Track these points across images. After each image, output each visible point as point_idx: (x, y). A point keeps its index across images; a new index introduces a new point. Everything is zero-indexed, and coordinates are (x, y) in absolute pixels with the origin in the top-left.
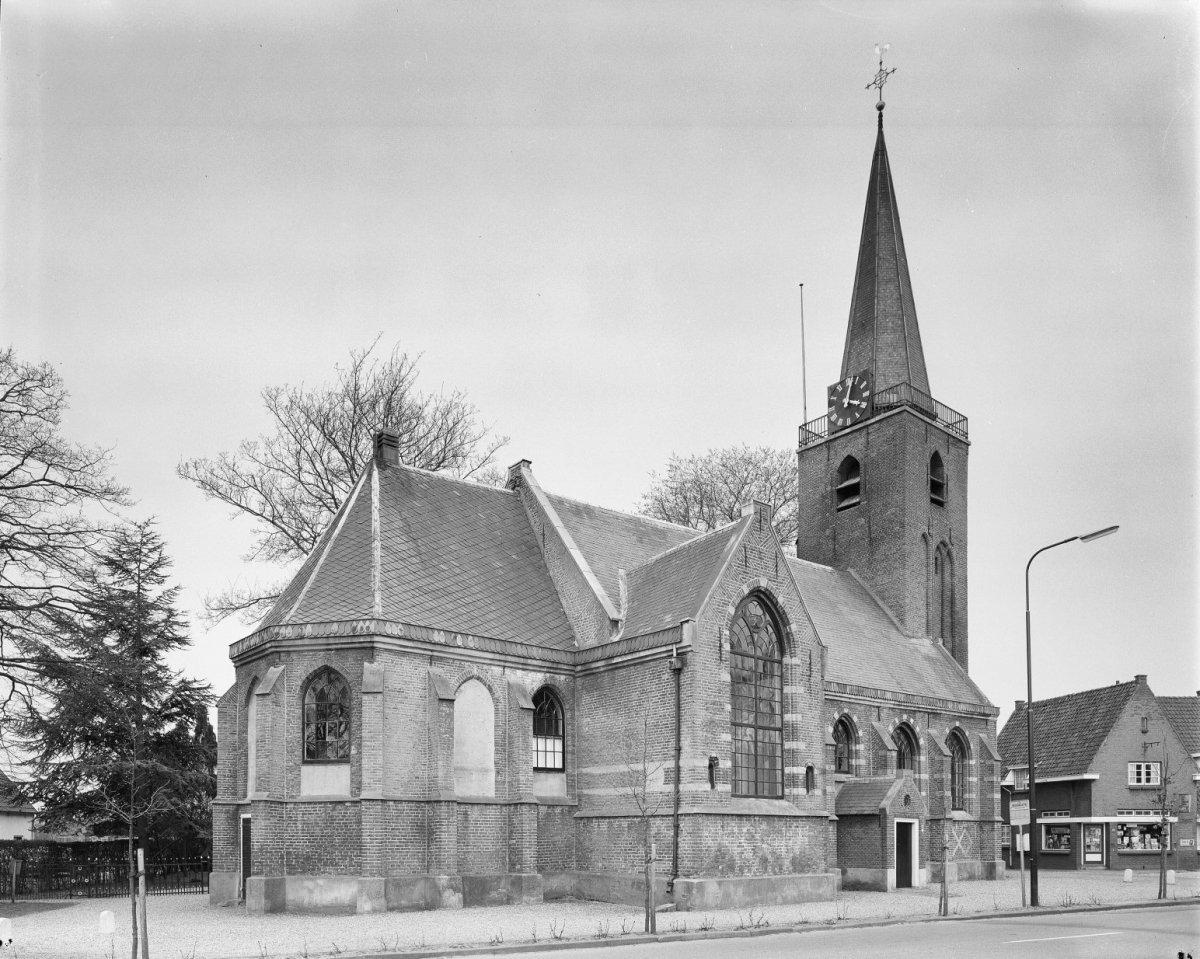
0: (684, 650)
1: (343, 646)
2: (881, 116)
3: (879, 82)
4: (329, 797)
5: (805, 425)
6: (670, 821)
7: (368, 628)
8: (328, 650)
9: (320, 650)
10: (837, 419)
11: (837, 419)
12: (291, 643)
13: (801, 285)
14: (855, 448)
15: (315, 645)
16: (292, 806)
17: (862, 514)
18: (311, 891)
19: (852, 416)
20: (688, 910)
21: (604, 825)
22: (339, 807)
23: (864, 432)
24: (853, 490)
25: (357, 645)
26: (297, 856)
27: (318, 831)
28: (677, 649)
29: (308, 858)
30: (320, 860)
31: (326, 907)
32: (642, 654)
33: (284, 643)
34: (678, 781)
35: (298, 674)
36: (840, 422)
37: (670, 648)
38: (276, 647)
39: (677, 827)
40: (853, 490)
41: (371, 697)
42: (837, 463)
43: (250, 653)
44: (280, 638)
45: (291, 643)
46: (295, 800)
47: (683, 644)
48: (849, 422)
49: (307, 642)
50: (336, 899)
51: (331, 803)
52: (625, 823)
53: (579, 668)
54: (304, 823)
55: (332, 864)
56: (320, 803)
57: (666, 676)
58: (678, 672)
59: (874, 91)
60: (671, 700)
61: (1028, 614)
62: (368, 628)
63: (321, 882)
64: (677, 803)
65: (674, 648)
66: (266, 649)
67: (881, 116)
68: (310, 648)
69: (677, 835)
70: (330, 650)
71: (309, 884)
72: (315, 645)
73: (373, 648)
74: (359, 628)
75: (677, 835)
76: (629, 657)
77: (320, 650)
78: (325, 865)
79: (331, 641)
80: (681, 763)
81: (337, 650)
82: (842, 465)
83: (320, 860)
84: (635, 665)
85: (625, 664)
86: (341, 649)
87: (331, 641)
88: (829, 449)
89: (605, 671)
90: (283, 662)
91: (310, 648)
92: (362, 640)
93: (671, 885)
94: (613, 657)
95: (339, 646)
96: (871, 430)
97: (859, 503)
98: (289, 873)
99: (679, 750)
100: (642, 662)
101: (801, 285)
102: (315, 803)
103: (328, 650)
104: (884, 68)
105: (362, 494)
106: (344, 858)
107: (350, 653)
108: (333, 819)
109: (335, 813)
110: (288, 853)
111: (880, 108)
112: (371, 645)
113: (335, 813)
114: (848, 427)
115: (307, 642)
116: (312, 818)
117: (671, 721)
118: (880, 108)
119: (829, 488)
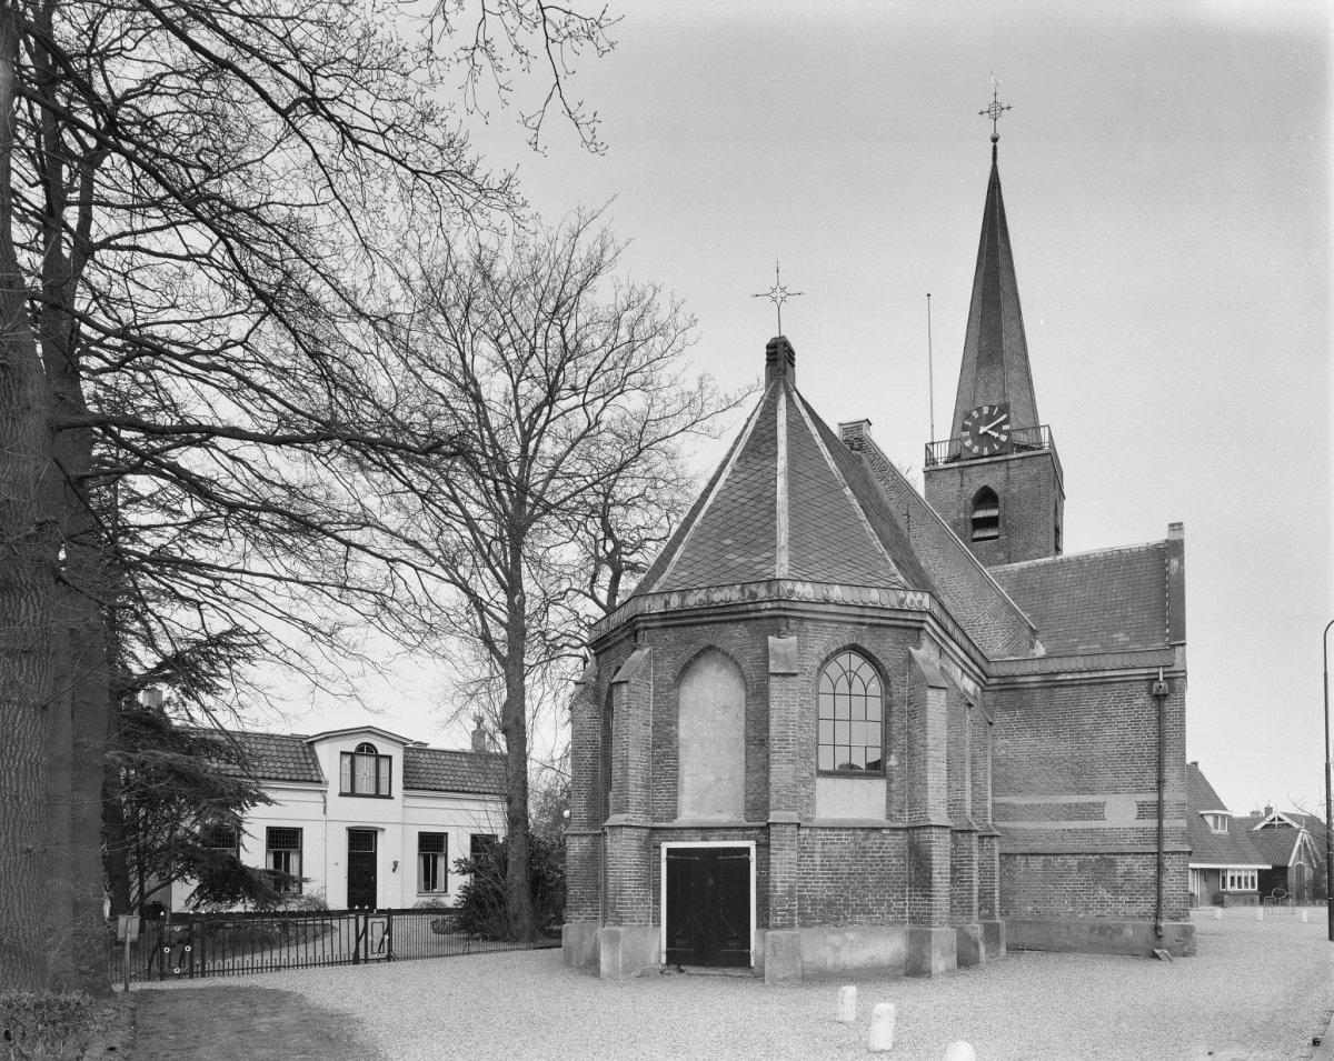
0: (1174, 675)
1: (882, 621)
2: (995, 148)
3: (995, 111)
4: (860, 821)
5: (933, 444)
6: (1151, 860)
7: (921, 602)
8: (859, 624)
9: (849, 623)
10: (973, 445)
11: (973, 445)
12: (809, 607)
13: (929, 295)
14: (994, 479)
15: (842, 614)
16: (807, 831)
17: (1001, 549)
18: (837, 949)
19: (991, 447)
20: (1185, 955)
21: (1037, 863)
22: (874, 835)
23: (1004, 465)
24: (991, 522)
25: (902, 623)
26: (814, 902)
27: (844, 868)
28: (1164, 673)
29: (830, 904)
30: (846, 907)
31: (857, 970)
32: (1108, 674)
33: (799, 606)
34: (1160, 816)
35: (816, 651)
36: (976, 449)
37: (1155, 670)
38: (785, 609)
39: (1159, 866)
40: (991, 522)
41: (935, 691)
42: (972, 491)
43: (684, 614)
44: (794, 598)
45: (809, 607)
46: (810, 824)
47: (1176, 668)
48: (986, 452)
49: (832, 608)
50: (872, 958)
51: (862, 829)
52: (1073, 861)
53: (994, 681)
54: (824, 855)
55: (863, 910)
56: (847, 829)
57: (1140, 701)
58: (1159, 698)
59: (987, 121)
60: (1152, 728)
61: (1326, 674)
62: (921, 602)
63: (851, 936)
64: (1159, 840)
65: (1161, 670)
66: (760, 611)
67: (995, 148)
68: (836, 618)
69: (1159, 873)
70: (863, 624)
71: (835, 939)
72: (842, 614)
73: (921, 629)
74: (908, 600)
75: (1159, 873)
76: (1087, 675)
77: (849, 623)
78: (854, 912)
79: (868, 612)
80: (1165, 797)
81: (871, 625)
82: (976, 495)
83: (846, 907)
84: (1080, 685)
85: (1076, 682)
86: (878, 625)
87: (868, 612)
88: (962, 475)
89: (1038, 688)
90: (793, 633)
91: (836, 618)
92: (910, 617)
93: (1157, 928)
94: (1058, 673)
95: (876, 621)
96: (1011, 464)
97: (996, 537)
98: (803, 925)
99: (1160, 782)
100: (1104, 682)
101: (929, 295)
102: (840, 829)
103: (859, 624)
104: (999, 100)
105: (762, 425)
106: (879, 903)
107: (889, 632)
108: (864, 851)
109: (868, 844)
110: (801, 898)
111: (995, 140)
112: (918, 625)
113: (868, 844)
114: (985, 457)
115: (832, 608)
116: (836, 849)
117: (1148, 750)
118: (995, 140)
119: (962, 516)
